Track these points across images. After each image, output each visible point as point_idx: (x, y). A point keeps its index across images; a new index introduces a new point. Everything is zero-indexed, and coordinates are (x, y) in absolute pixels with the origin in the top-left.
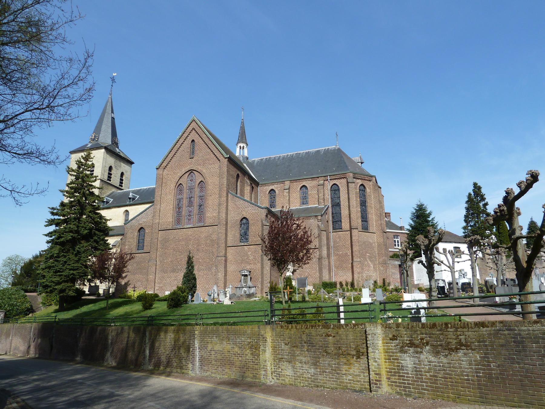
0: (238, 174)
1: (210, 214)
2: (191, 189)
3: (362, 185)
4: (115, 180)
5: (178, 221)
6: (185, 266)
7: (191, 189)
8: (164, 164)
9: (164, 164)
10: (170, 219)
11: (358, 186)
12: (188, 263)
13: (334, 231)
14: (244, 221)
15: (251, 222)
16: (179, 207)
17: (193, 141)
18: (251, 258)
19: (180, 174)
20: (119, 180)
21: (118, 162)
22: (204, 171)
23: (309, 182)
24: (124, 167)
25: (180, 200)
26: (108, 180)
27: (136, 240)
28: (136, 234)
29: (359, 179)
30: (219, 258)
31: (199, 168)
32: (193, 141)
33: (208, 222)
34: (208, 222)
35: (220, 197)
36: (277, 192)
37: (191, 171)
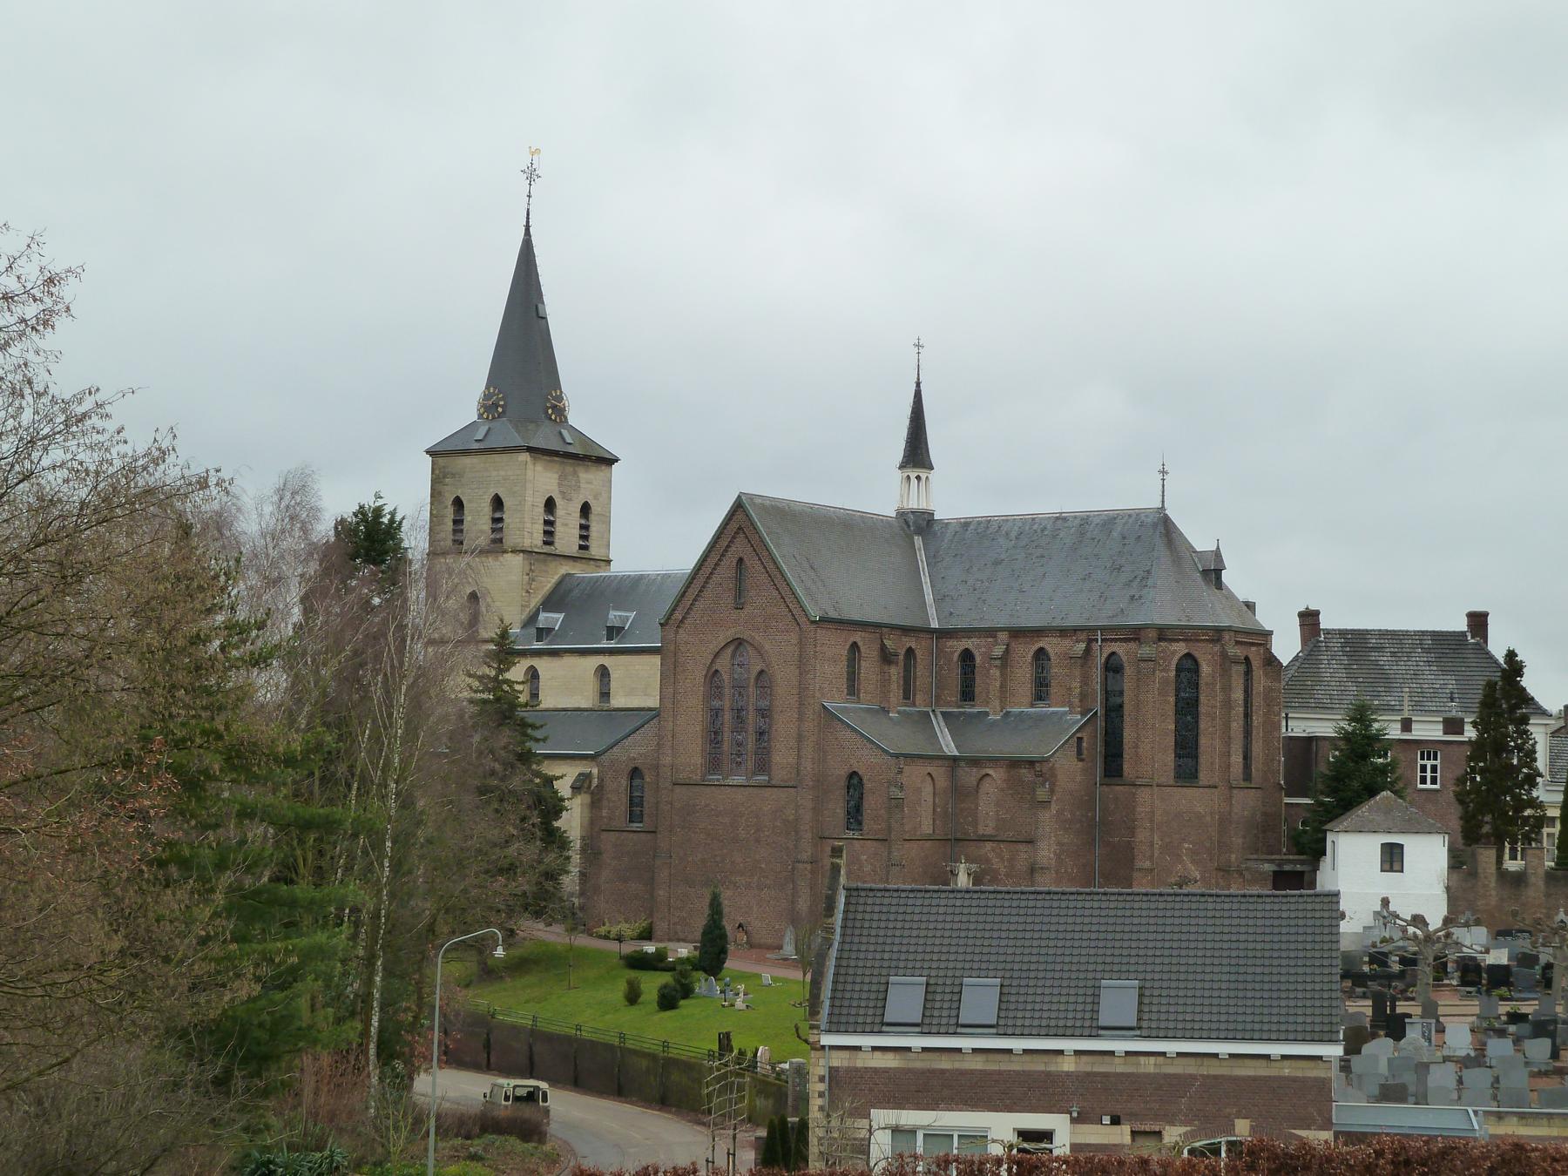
0: (855, 645)
1: (782, 757)
2: (739, 687)
3: (1188, 655)
4: (567, 538)
5: (714, 763)
6: (707, 911)
7: (739, 687)
8: (678, 615)
9: (678, 615)
10: (698, 760)
11: (1175, 662)
12: (711, 905)
13: (1107, 780)
14: (855, 781)
15: (868, 785)
16: (713, 736)
17: (741, 560)
18: (868, 868)
19: (714, 647)
20: (577, 532)
21: (569, 469)
22: (767, 647)
23: (1055, 640)
24: (589, 478)
25: (716, 713)
26: (545, 543)
27: (625, 800)
28: (624, 782)
29: (1178, 641)
30: (800, 866)
31: (758, 637)
32: (741, 560)
33: (779, 775)
34: (779, 775)
35: (801, 719)
36: (978, 659)
37: (738, 642)
